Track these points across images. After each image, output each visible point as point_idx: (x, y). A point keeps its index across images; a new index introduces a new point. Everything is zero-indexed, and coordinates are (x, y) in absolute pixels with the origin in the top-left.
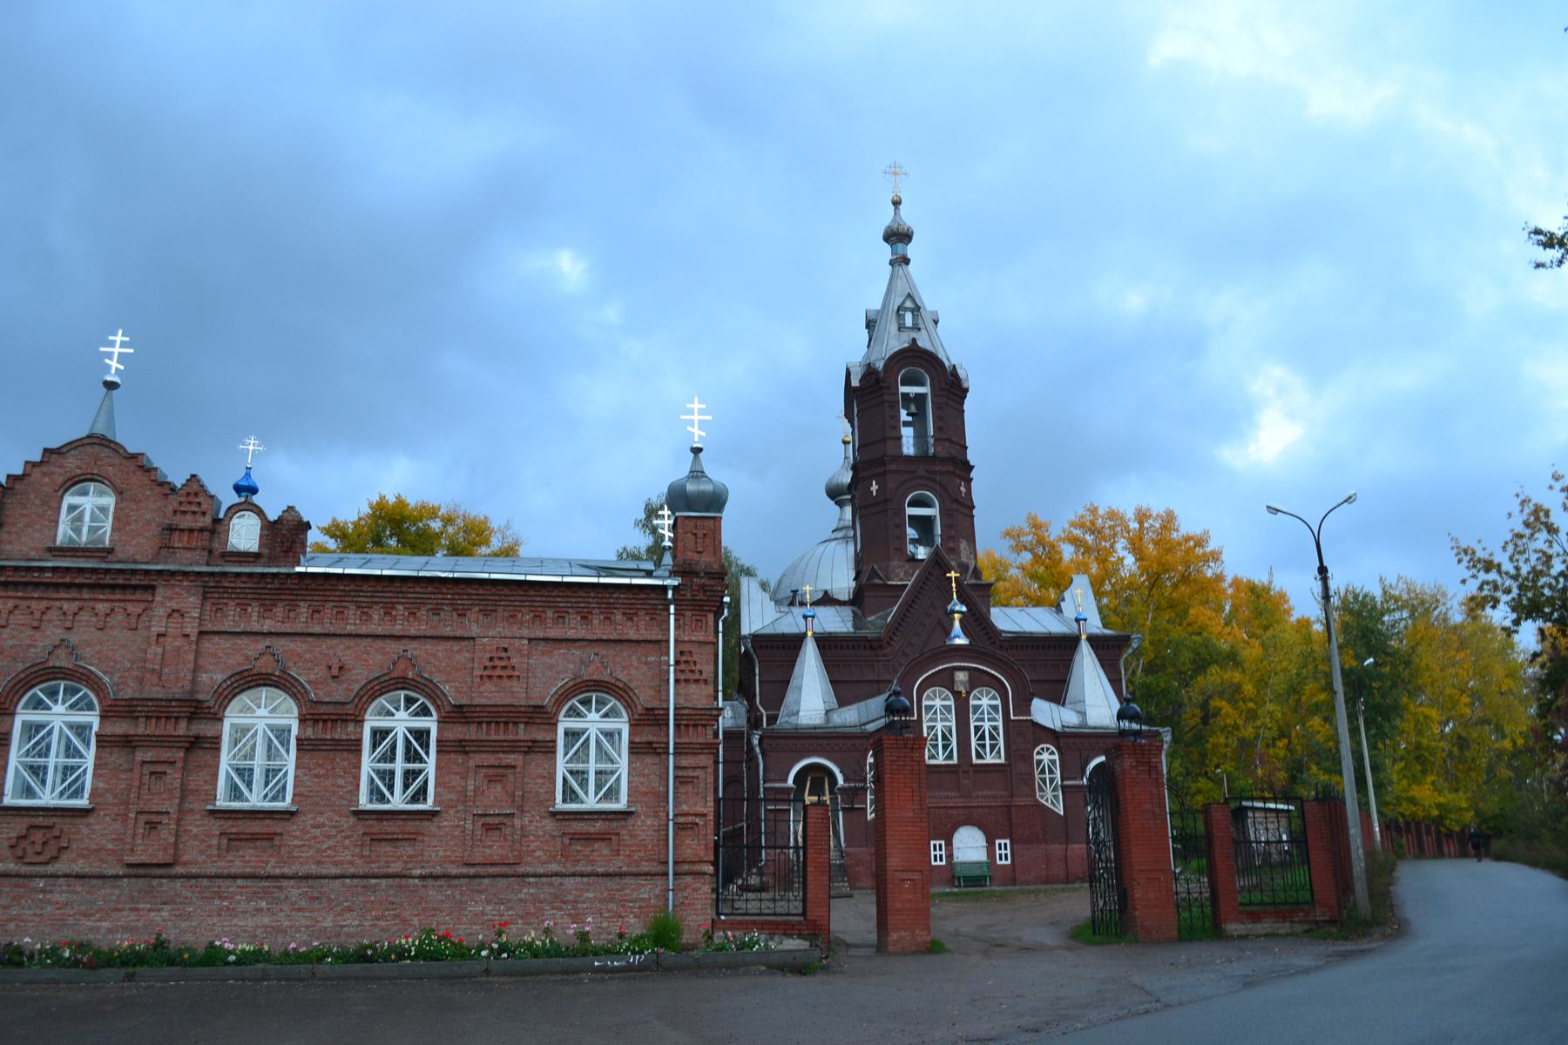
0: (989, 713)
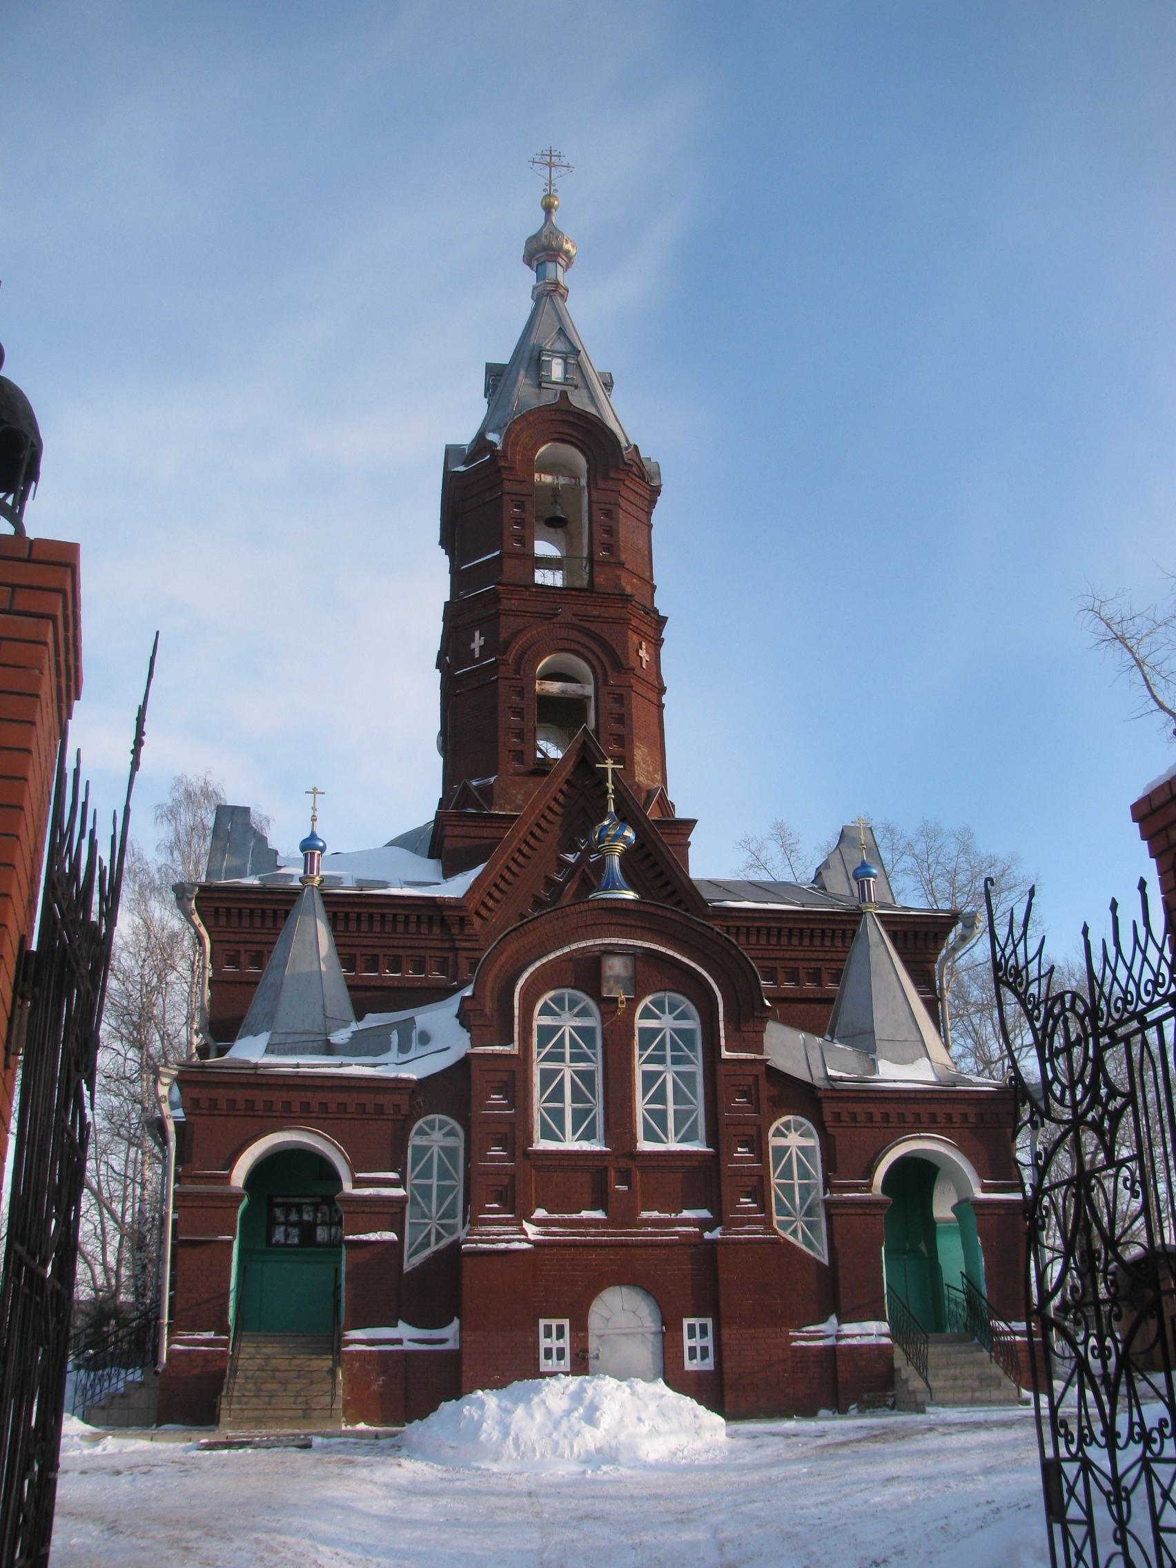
0: (574, 1044)
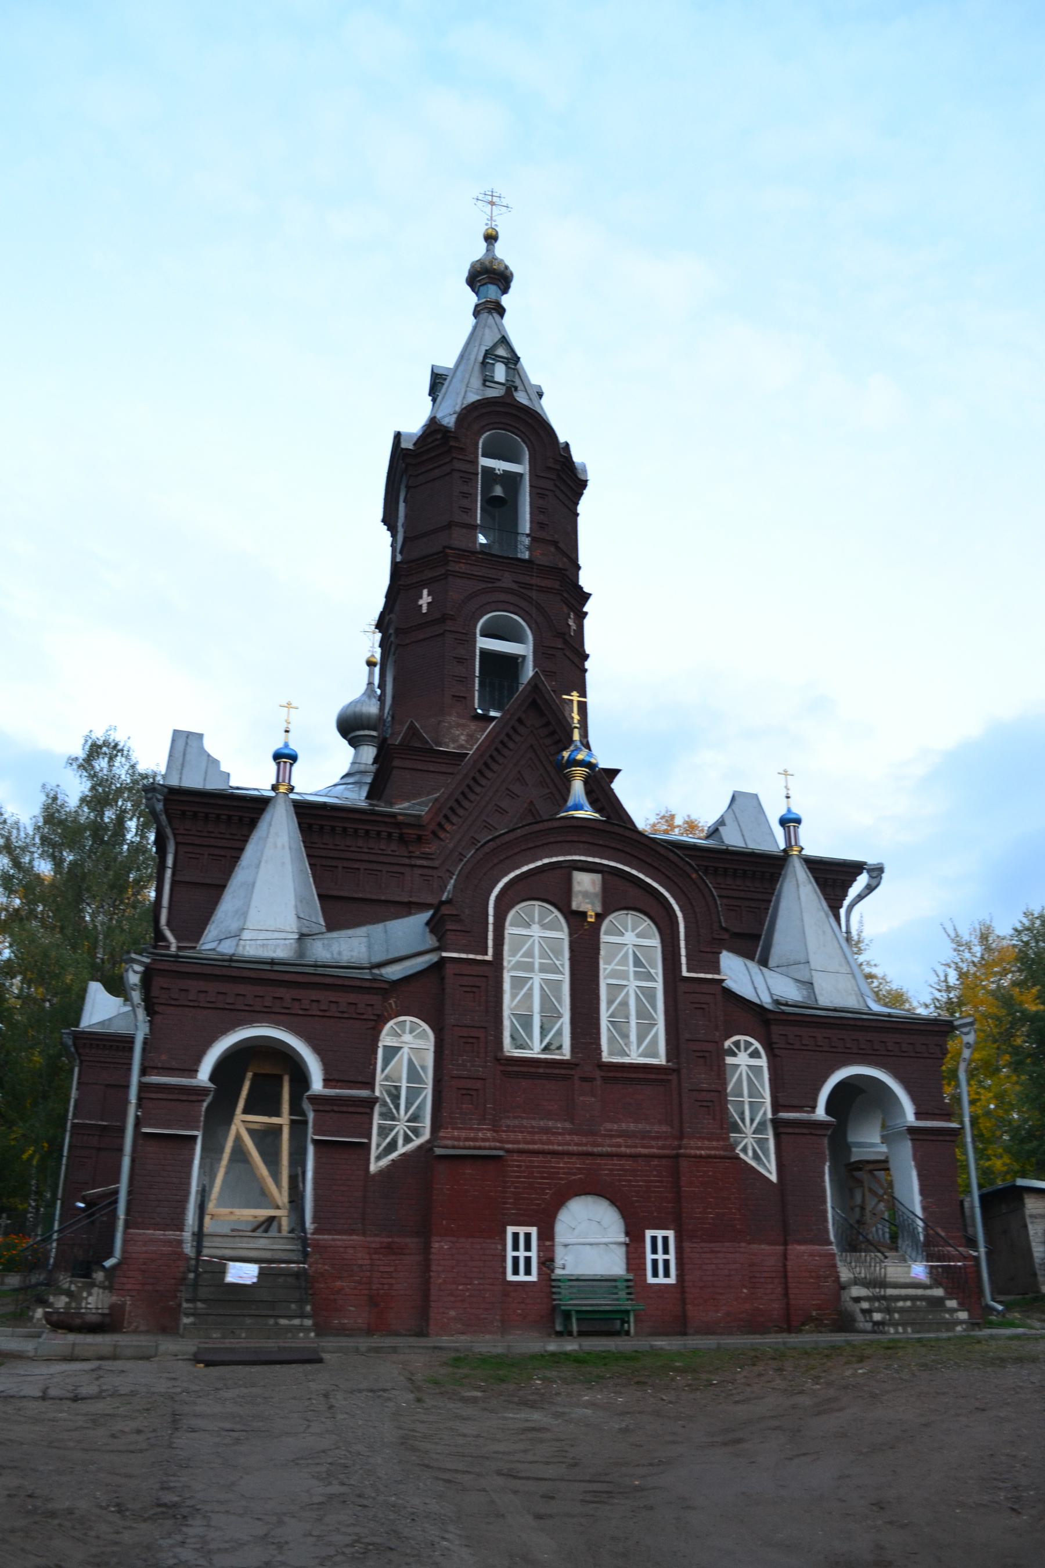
0: (544, 955)
